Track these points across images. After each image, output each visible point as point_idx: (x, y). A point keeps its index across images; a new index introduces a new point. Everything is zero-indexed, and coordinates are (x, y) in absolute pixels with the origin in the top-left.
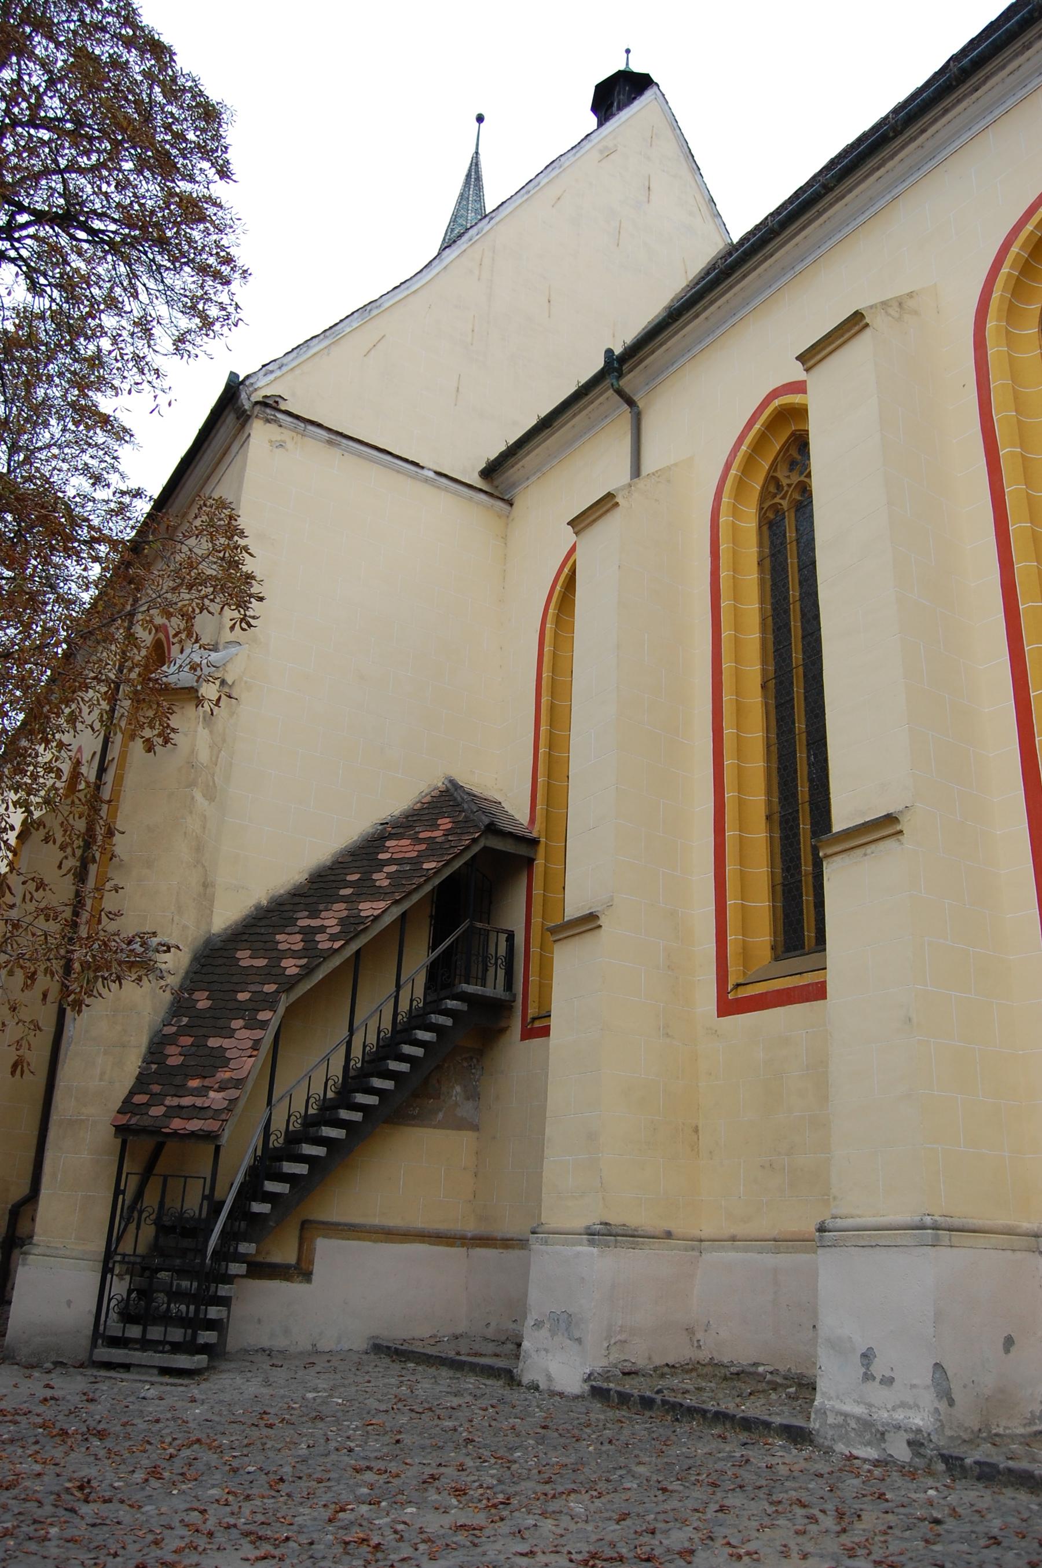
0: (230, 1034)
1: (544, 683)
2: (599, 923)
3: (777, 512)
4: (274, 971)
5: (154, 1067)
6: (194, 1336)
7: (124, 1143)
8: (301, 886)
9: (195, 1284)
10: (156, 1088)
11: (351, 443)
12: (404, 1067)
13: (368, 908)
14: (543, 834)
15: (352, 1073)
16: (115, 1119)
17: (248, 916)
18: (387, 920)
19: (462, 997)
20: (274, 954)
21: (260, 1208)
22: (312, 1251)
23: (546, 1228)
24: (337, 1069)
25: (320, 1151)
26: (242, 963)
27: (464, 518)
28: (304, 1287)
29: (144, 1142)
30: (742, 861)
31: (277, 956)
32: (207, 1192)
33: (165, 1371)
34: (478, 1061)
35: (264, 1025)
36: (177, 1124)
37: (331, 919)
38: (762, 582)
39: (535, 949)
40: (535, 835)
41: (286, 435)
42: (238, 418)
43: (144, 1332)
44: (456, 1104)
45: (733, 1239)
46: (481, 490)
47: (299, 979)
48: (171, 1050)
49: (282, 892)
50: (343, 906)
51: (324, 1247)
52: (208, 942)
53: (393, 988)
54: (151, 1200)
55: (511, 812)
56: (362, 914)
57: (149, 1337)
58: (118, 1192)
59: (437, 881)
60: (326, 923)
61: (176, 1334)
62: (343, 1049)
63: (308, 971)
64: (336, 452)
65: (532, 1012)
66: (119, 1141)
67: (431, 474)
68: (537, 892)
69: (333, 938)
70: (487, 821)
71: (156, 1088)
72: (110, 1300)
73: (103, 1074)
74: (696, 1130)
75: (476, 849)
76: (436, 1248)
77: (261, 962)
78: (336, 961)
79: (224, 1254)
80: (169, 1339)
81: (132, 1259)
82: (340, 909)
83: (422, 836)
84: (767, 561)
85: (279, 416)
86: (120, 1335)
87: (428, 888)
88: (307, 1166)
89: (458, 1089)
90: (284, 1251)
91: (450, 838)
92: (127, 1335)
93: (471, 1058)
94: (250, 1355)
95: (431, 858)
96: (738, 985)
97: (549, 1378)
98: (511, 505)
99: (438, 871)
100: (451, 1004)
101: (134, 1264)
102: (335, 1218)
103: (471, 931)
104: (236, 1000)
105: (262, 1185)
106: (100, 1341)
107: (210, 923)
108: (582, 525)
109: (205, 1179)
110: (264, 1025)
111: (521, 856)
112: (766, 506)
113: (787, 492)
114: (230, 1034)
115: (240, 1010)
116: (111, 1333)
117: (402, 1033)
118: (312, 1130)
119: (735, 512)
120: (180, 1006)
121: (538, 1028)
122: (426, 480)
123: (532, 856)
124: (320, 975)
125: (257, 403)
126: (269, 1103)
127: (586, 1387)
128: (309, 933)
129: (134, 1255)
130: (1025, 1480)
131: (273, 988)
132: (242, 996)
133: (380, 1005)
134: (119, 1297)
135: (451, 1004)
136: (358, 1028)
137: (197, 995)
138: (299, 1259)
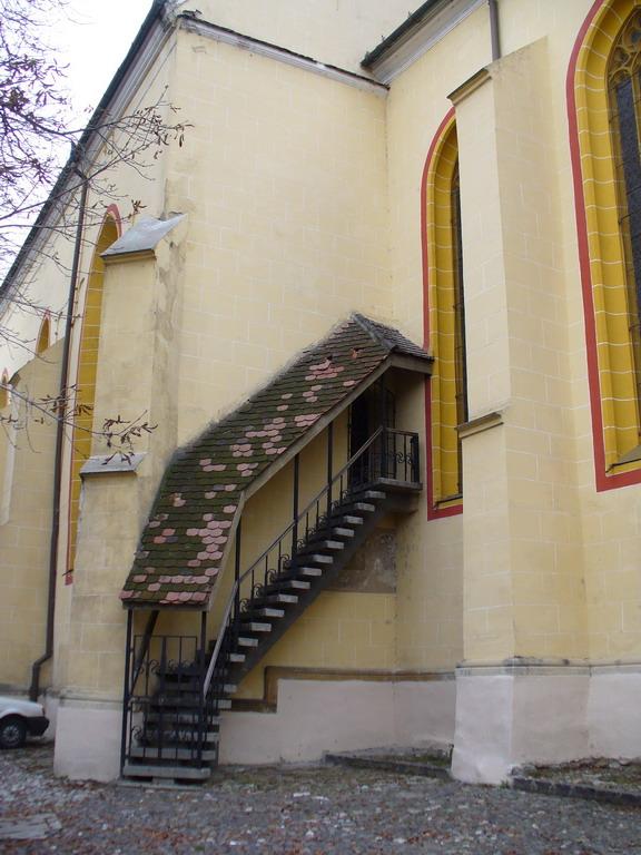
1: (428, 231)
2: (501, 421)
3: (622, 77)
4: (233, 474)
6: (200, 755)
7: (130, 613)
8: (245, 406)
9: (196, 717)
10: (151, 570)
11: (258, 45)
12: (339, 545)
13: (302, 420)
14: (437, 354)
15: (299, 552)
17: (203, 435)
18: (319, 429)
21: (235, 658)
22: (275, 689)
23: (468, 662)
24: (287, 550)
25: (279, 613)
26: (205, 469)
27: (339, 104)
28: (271, 715)
29: (145, 612)
30: (612, 366)
33: (180, 781)
35: (229, 517)
36: (171, 596)
37: (273, 430)
38: (613, 136)
39: (435, 447)
40: (430, 354)
41: (205, 42)
42: (164, 31)
43: (160, 753)
44: (377, 574)
45: (618, 663)
46: (363, 78)
47: (254, 478)
49: (230, 411)
50: (282, 420)
51: (284, 687)
53: (326, 483)
54: (155, 654)
55: (407, 338)
56: (298, 425)
57: (163, 756)
58: (128, 651)
59: (356, 396)
60: (270, 434)
61: (185, 754)
63: (259, 474)
64: (246, 53)
65: (436, 497)
66: (127, 611)
67: (322, 67)
68: (435, 401)
69: (277, 445)
70: (392, 345)
73: (107, 560)
74: (583, 581)
75: (385, 368)
77: (221, 468)
78: (281, 464)
79: (216, 693)
82: (279, 422)
84: (616, 120)
85: (200, 26)
86: (141, 755)
87: (349, 402)
88: (270, 625)
89: (378, 561)
90: (254, 691)
96: (614, 465)
97: (478, 775)
98: (388, 89)
99: (356, 388)
100: (373, 494)
101: (145, 702)
102: (290, 664)
103: (384, 436)
106: (127, 761)
107: (176, 440)
108: (460, 98)
110: (229, 517)
111: (419, 373)
112: (613, 73)
113: (632, 59)
117: (335, 517)
118: (271, 597)
119: (587, 80)
120: (161, 505)
121: (449, 507)
122: (319, 72)
124: (269, 474)
125: (179, 16)
126: (237, 577)
127: (510, 781)
128: (257, 444)
130: (629, 802)
131: (232, 487)
133: (318, 493)
134: (138, 728)
135: (373, 494)
136: (302, 516)
138: (265, 697)
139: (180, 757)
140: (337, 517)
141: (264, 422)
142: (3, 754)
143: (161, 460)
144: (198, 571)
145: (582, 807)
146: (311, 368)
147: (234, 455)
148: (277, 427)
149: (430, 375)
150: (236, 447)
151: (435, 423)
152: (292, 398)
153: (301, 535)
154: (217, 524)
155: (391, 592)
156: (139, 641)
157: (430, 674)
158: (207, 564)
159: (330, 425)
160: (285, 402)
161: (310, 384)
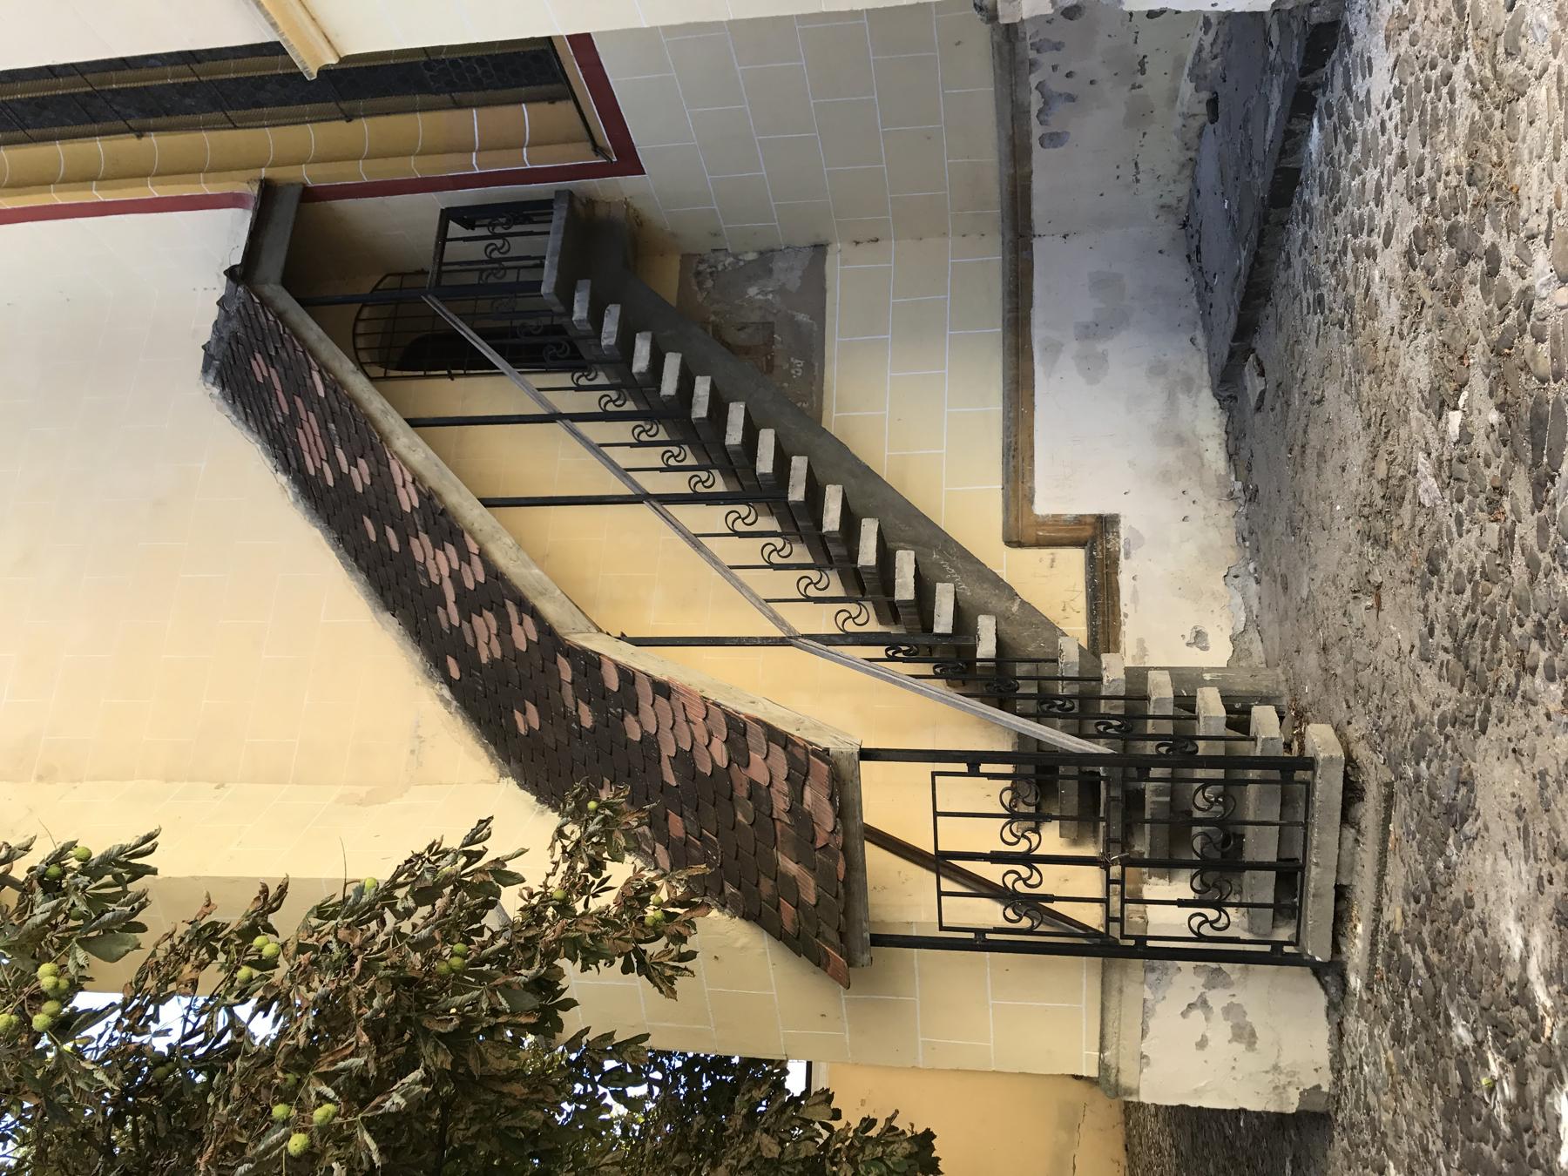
0: (650, 742)
5: (729, 889)
14: (254, 173)
15: (736, 487)
19: (565, 293)
25: (869, 531)
32: (963, 767)
39: (476, 164)
40: (254, 190)
50: (414, 543)
60: (445, 572)
62: (673, 509)
68: (362, 172)
71: (766, 886)
76: (1036, 301)
80: (1274, 814)
81: (1115, 902)
93: (698, 273)
95: (309, 382)
100: (580, 311)
109: (934, 774)
114: (650, 742)
115: (610, 726)
118: (834, 550)
123: (298, 191)
132: (587, 720)
135: (580, 311)
146: (312, 472)
149: (1299, 171)
151: (414, 168)
155: (824, 254)
159: (414, 423)
161: (343, 480)
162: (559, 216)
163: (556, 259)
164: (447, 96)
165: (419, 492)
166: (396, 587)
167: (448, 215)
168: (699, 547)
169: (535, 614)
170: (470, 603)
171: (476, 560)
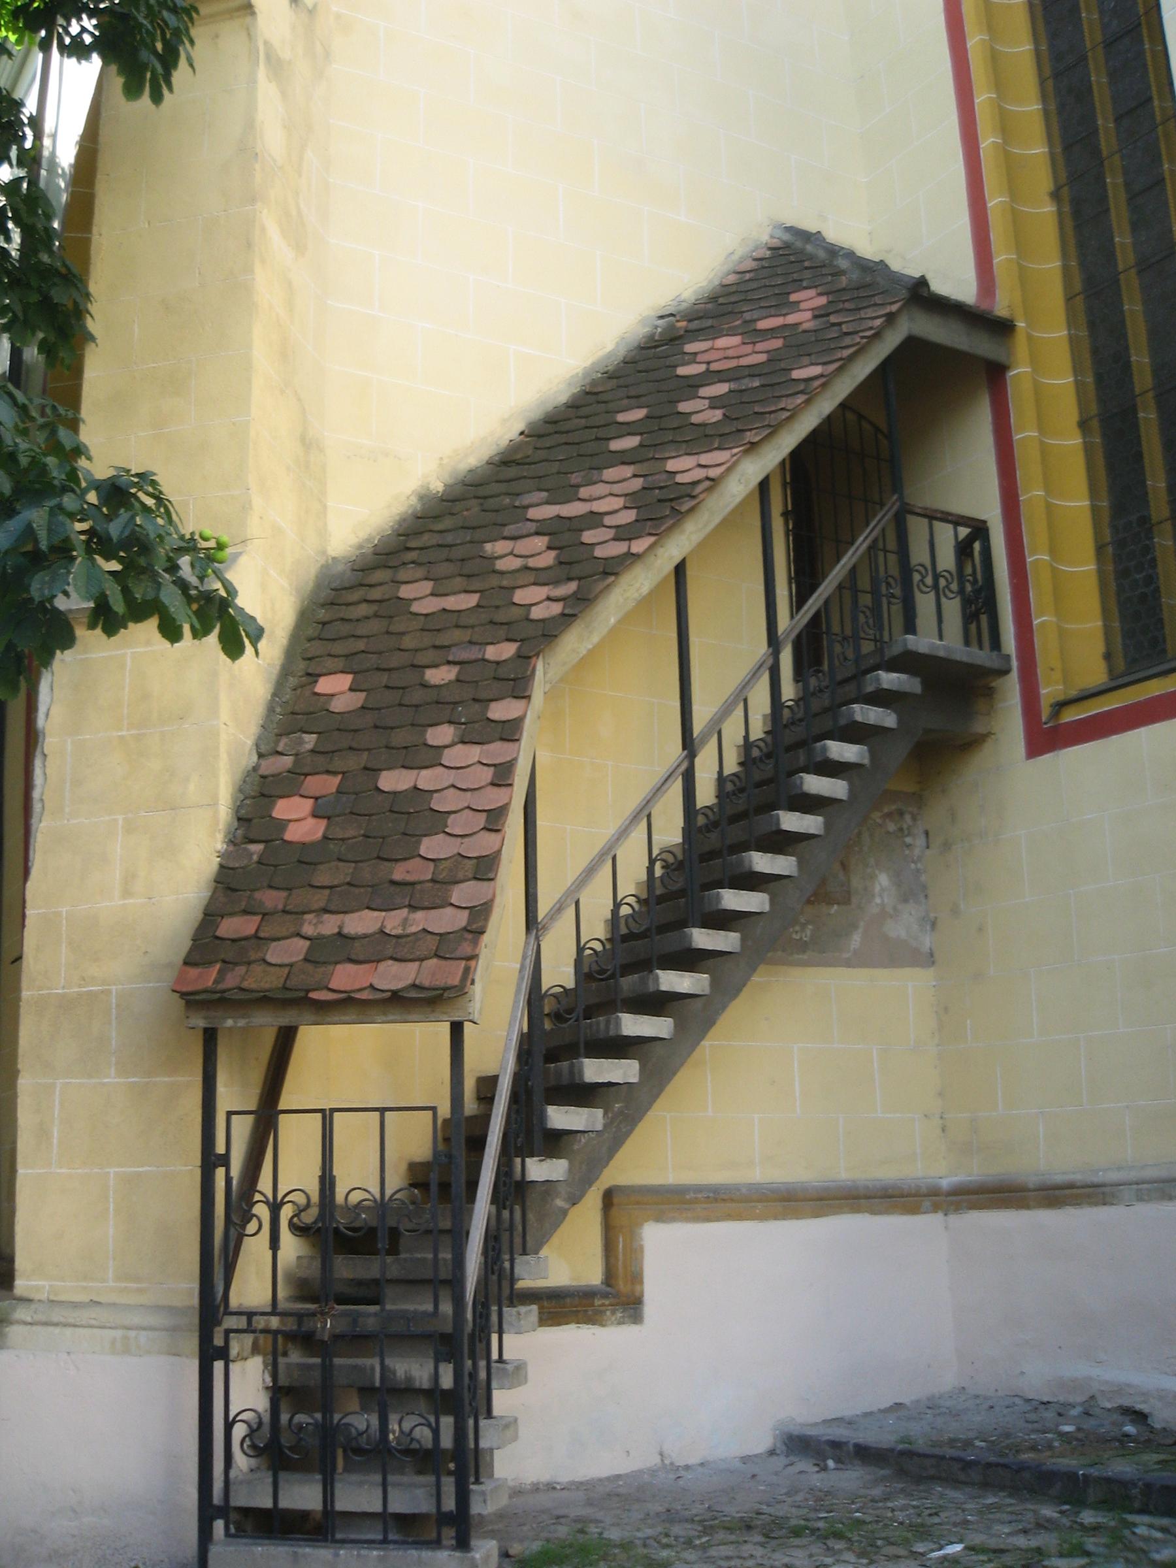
5: (257, 848)
8: (513, 447)
16: (180, 979)
17: (403, 520)
20: (494, 581)
22: (635, 1252)
31: (497, 590)
34: (914, 819)
39: (1037, 557)
40: (1001, 309)
48: (283, 809)
50: (628, 471)
51: (662, 1245)
52: (325, 567)
56: (680, 479)
62: (677, 786)
65: (1050, 691)
68: (1024, 434)
71: (271, 899)
72: (229, 1426)
73: (129, 878)
83: (763, 325)
86: (268, 1503)
89: (883, 879)
91: (833, 319)
92: (284, 1504)
93: (901, 813)
94: (22, 1300)
95: (806, 360)
100: (889, 679)
104: (425, 686)
105: (543, 1117)
106: (219, 1525)
114: (432, 757)
115: (441, 706)
116: (240, 1499)
120: (293, 712)
128: (563, 534)
129: (274, 1311)
137: (324, 685)
138: (609, 1276)
139: (399, 1504)
140: (802, 744)
141: (575, 479)
142: (1031, 6)
143: (285, 583)
144: (412, 896)
145: (1116, 1448)
147: (501, 565)
148: (616, 489)
150: (501, 547)
151: (1032, 494)
152: (647, 417)
153: (706, 795)
154: (474, 753)
156: (242, 1128)
157: (1071, 1186)
158: (444, 880)
160: (629, 429)
161: (691, 386)
162: (981, 656)
163: (942, 654)
164: (1109, 539)
165: (695, 483)
166: (563, 441)
167: (980, 530)
168: (635, 818)
169: (567, 619)
170: (563, 534)
171: (619, 548)
